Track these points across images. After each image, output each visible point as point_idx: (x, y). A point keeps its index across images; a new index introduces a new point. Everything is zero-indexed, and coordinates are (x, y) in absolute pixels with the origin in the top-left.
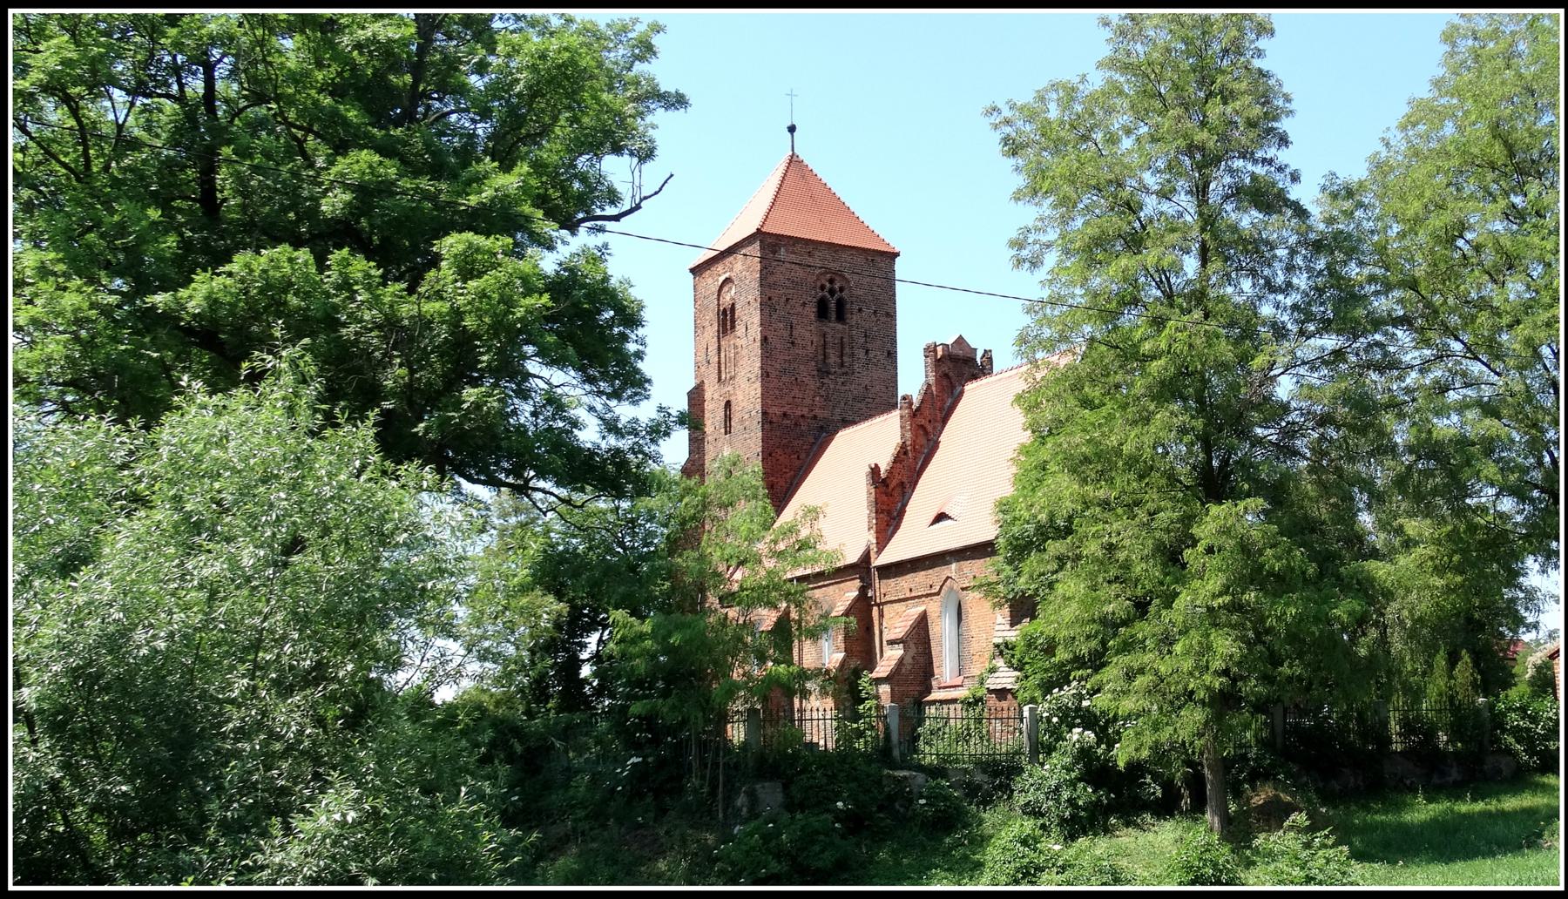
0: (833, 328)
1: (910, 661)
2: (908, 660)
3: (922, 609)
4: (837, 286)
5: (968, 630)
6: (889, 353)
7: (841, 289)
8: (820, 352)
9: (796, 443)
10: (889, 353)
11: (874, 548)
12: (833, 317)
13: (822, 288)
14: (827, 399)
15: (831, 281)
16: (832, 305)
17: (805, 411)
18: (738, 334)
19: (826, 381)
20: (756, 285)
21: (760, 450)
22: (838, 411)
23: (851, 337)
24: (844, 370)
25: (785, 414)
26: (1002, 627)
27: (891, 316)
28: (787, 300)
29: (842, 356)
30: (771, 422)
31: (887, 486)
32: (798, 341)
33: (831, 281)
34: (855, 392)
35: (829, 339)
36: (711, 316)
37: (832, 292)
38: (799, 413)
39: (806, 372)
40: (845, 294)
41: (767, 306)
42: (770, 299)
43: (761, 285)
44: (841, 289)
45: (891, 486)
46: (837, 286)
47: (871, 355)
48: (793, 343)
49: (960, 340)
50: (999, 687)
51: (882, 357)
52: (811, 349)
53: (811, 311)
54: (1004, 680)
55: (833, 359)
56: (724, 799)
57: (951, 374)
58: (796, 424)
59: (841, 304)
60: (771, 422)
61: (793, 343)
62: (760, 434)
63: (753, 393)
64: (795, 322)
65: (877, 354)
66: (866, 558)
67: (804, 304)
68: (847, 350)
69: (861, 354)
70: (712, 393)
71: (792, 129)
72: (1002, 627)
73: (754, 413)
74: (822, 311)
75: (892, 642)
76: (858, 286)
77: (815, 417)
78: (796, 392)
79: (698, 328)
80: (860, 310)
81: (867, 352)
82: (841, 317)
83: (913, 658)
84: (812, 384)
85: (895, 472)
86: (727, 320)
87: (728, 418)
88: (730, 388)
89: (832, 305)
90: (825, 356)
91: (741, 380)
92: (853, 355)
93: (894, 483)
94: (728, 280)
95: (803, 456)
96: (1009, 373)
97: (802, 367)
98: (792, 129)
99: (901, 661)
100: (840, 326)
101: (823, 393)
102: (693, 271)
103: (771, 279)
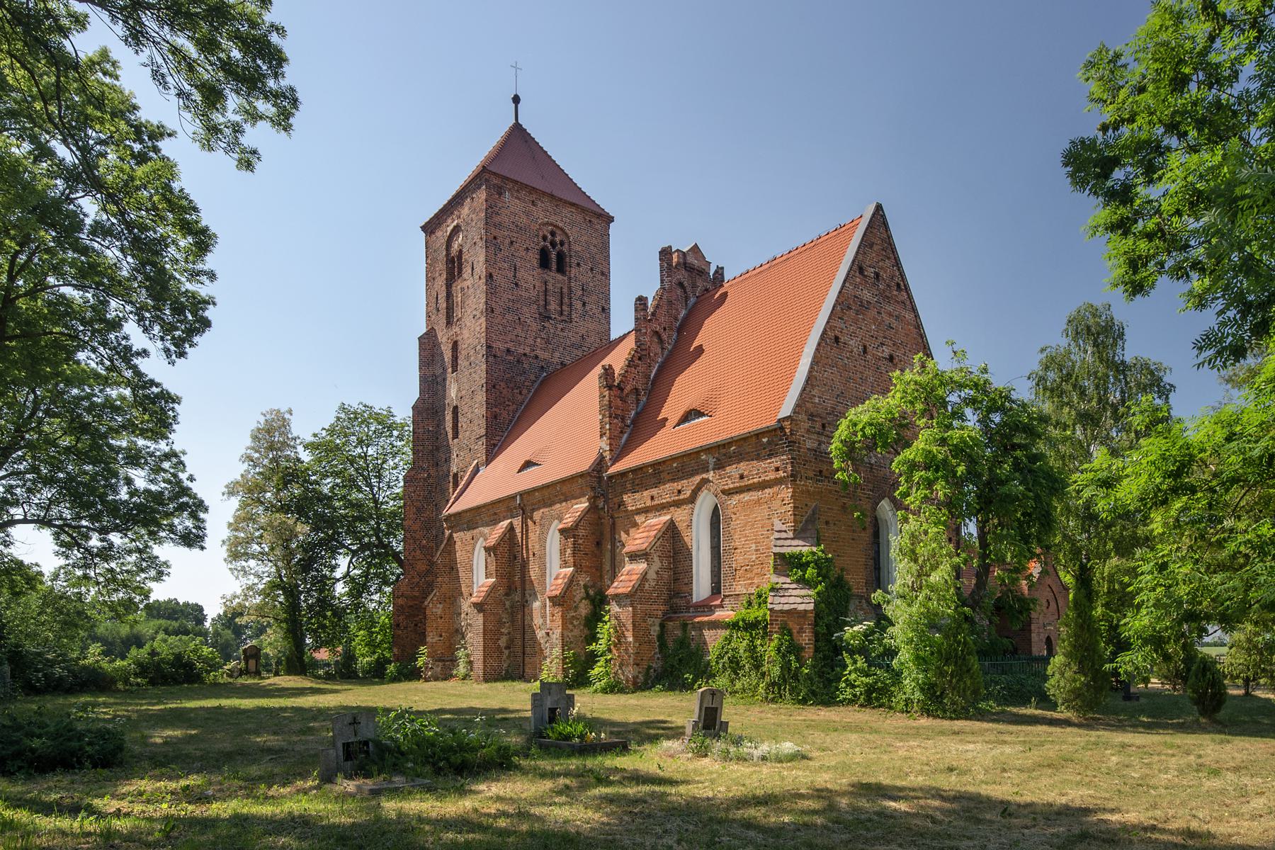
0: (553, 277)
1: (655, 576)
2: (652, 575)
3: (668, 517)
4: (558, 239)
5: (730, 538)
6: (603, 309)
7: (562, 243)
8: (542, 297)
9: (518, 378)
10: (603, 309)
11: (607, 455)
12: (554, 267)
13: (545, 238)
14: (548, 342)
15: (553, 234)
16: (553, 256)
17: (528, 350)
18: (465, 276)
19: (546, 325)
20: (481, 224)
21: (483, 431)
22: (557, 354)
23: (570, 288)
24: (564, 318)
25: (508, 350)
26: (784, 535)
27: (606, 274)
28: (512, 242)
29: (561, 304)
30: (495, 356)
31: (622, 390)
32: (521, 283)
33: (553, 234)
34: (573, 339)
35: (550, 287)
36: (441, 266)
37: (553, 244)
38: (522, 351)
39: (529, 313)
40: (565, 249)
41: (492, 243)
42: (495, 238)
43: (487, 223)
44: (562, 243)
45: (626, 391)
46: (558, 239)
47: (588, 308)
48: (517, 284)
49: (696, 249)
50: (786, 607)
51: (597, 311)
52: (533, 293)
53: (534, 257)
54: (792, 600)
55: (553, 306)
56: (1161, 834)
57: (686, 284)
58: (518, 361)
59: (561, 256)
60: (495, 356)
61: (517, 284)
62: (484, 366)
63: (478, 329)
64: (518, 265)
65: (593, 308)
66: (600, 464)
67: (527, 249)
68: (566, 300)
69: (578, 305)
70: (443, 337)
71: (516, 100)
72: (784, 535)
73: (479, 347)
74: (544, 262)
75: (634, 557)
76: (578, 236)
77: (537, 357)
78: (519, 331)
79: (430, 280)
80: (578, 265)
81: (584, 304)
82: (561, 269)
83: (657, 573)
84: (535, 326)
85: (631, 376)
86: (454, 266)
87: (455, 358)
88: (457, 329)
89: (553, 256)
90: (546, 303)
91: (468, 321)
92: (571, 305)
93: (628, 388)
94: (457, 229)
95: (525, 391)
96: (747, 275)
97: (525, 309)
98: (516, 100)
99: (644, 577)
100: (559, 277)
101: (545, 336)
102: (424, 228)
103: (497, 219)
